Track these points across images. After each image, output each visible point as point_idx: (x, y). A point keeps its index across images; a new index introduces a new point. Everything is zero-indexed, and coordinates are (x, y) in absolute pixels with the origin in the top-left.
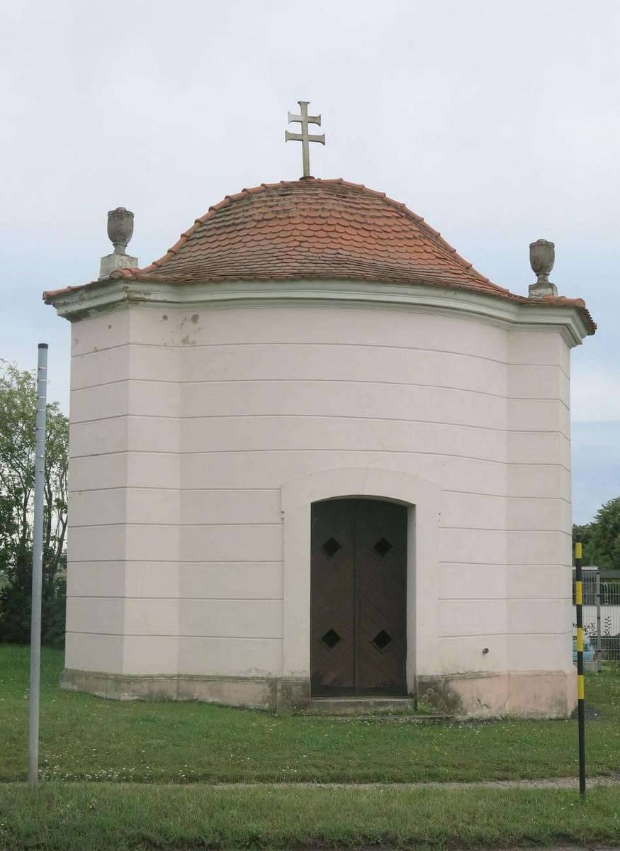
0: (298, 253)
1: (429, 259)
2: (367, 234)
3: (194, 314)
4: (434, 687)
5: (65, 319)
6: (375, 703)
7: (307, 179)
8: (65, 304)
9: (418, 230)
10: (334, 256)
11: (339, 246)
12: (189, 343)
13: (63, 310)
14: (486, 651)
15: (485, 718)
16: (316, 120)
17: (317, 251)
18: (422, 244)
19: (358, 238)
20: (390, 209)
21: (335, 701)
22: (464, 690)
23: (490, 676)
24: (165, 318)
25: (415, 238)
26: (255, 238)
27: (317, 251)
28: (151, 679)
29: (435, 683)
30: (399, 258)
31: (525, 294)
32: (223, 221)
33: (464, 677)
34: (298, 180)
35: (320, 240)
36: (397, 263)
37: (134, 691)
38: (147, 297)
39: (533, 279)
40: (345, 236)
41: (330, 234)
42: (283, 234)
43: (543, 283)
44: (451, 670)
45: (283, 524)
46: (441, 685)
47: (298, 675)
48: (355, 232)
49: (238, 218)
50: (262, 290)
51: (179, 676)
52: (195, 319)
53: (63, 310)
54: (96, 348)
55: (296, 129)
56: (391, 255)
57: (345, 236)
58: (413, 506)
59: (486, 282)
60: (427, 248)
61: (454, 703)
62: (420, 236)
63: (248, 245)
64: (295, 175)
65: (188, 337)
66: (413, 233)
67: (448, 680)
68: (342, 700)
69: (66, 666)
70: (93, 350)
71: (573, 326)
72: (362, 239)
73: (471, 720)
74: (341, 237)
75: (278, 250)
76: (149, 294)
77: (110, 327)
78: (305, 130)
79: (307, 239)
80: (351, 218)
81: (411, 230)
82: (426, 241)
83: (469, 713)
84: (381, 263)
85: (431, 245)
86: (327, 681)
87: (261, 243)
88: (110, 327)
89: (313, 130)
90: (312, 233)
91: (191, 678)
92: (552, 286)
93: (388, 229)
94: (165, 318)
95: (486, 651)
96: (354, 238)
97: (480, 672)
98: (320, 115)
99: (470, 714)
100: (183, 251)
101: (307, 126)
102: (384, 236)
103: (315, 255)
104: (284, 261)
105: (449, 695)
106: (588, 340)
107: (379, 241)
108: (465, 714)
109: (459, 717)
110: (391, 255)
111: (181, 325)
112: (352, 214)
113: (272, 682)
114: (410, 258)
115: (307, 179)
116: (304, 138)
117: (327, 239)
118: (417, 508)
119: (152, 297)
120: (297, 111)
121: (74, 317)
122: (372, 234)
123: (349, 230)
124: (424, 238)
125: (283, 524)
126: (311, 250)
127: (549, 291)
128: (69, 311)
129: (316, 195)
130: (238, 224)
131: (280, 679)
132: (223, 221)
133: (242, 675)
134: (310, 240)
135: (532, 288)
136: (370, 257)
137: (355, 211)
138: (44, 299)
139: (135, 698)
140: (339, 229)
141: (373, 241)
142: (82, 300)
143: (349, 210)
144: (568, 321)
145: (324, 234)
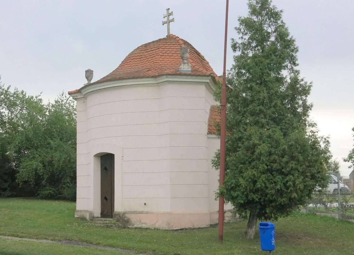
4: (119, 215)
6: (104, 220)
14: (145, 204)
15: (143, 228)
22: (133, 218)
26: (176, 62)
29: (119, 214)
37: (77, 214)
38: (77, 98)
44: (128, 210)
46: (121, 215)
50: (104, 86)
61: (128, 221)
64: (164, 35)
67: (124, 213)
69: (115, 210)
73: (136, 228)
75: (176, 64)
83: (135, 225)
86: (105, 213)
94: (84, 102)
95: (145, 204)
97: (143, 211)
99: (136, 226)
105: (125, 219)
108: (133, 225)
109: (130, 227)
117: (177, 57)
139: (78, 217)
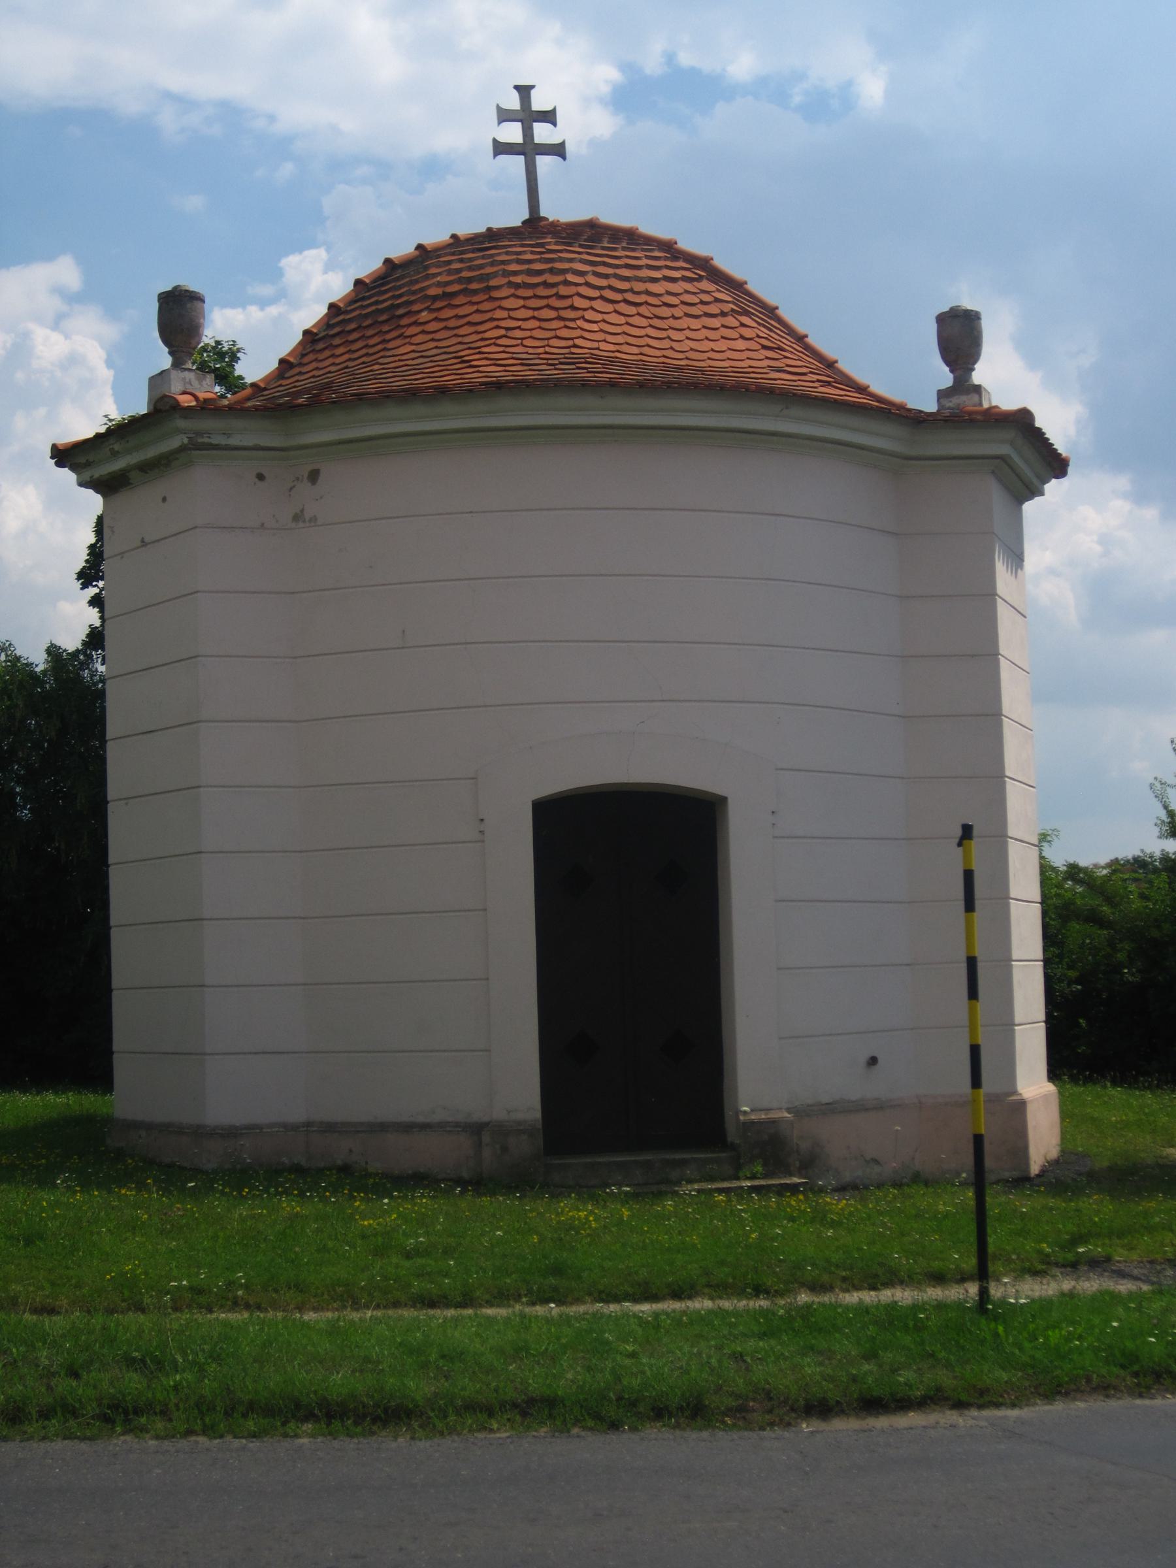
0: (501, 349)
1: (748, 350)
2: (632, 310)
3: (310, 467)
5: (91, 491)
7: (535, 224)
8: (88, 464)
9: (730, 299)
10: (566, 351)
11: (578, 333)
12: (304, 521)
13: (87, 475)
14: (873, 1061)
16: (549, 117)
17: (537, 343)
18: (737, 324)
19: (613, 318)
20: (681, 264)
21: (633, 1159)
23: (880, 1106)
24: (261, 477)
25: (723, 314)
27: (537, 343)
28: (253, 1129)
30: (691, 349)
31: (930, 405)
32: (377, 303)
33: (830, 1109)
34: (520, 224)
35: (545, 325)
36: (687, 358)
39: (946, 378)
40: (589, 315)
41: (563, 314)
42: (476, 318)
43: (963, 385)
45: (483, 841)
47: (520, 1116)
48: (609, 307)
49: (401, 296)
51: (308, 1124)
52: (314, 476)
53: (87, 475)
54: (143, 541)
55: (513, 133)
56: (676, 346)
57: (589, 315)
58: (723, 800)
59: (862, 390)
60: (747, 333)
62: (733, 310)
63: (414, 340)
64: (515, 215)
65: (302, 511)
66: (719, 305)
68: (600, 1160)
70: (139, 544)
71: (1017, 459)
72: (622, 320)
74: (583, 317)
76: (229, 435)
77: (164, 499)
78: (528, 133)
79: (520, 323)
80: (603, 282)
81: (717, 300)
82: (746, 320)
84: (653, 356)
85: (755, 325)
87: (437, 336)
88: (164, 499)
89: (543, 133)
90: (530, 313)
91: (330, 1128)
92: (978, 389)
93: (674, 300)
95: (873, 1061)
96: (606, 317)
98: (517, 87)
100: (306, 360)
101: (531, 128)
102: (665, 312)
103: (531, 351)
104: (473, 363)
106: (1053, 487)
107: (656, 322)
110: (676, 346)
111: (291, 489)
112: (606, 276)
113: (476, 1129)
114: (712, 350)
115: (535, 224)
116: (529, 150)
118: (730, 801)
119: (234, 441)
120: (513, 102)
121: (106, 486)
122: (643, 310)
123: (598, 305)
124: (740, 314)
125: (483, 841)
126: (527, 342)
127: (975, 398)
128: (96, 475)
129: (542, 245)
130: (399, 306)
131: (487, 1124)
132: (377, 303)
133: (421, 1119)
134: (524, 325)
135: (942, 395)
136: (635, 350)
137: (610, 271)
138: (52, 458)
140: (578, 302)
141: (644, 322)
142: (115, 454)
143: (601, 269)
144: (1004, 450)
145: (553, 314)
